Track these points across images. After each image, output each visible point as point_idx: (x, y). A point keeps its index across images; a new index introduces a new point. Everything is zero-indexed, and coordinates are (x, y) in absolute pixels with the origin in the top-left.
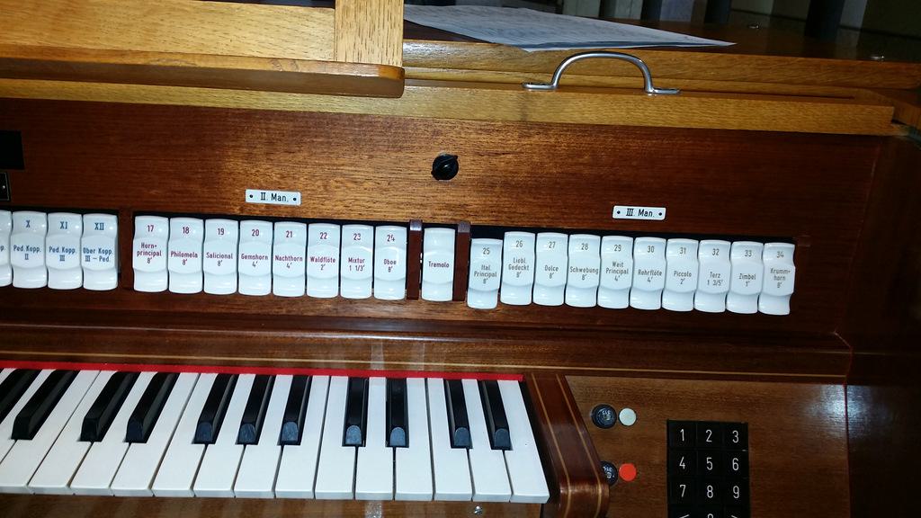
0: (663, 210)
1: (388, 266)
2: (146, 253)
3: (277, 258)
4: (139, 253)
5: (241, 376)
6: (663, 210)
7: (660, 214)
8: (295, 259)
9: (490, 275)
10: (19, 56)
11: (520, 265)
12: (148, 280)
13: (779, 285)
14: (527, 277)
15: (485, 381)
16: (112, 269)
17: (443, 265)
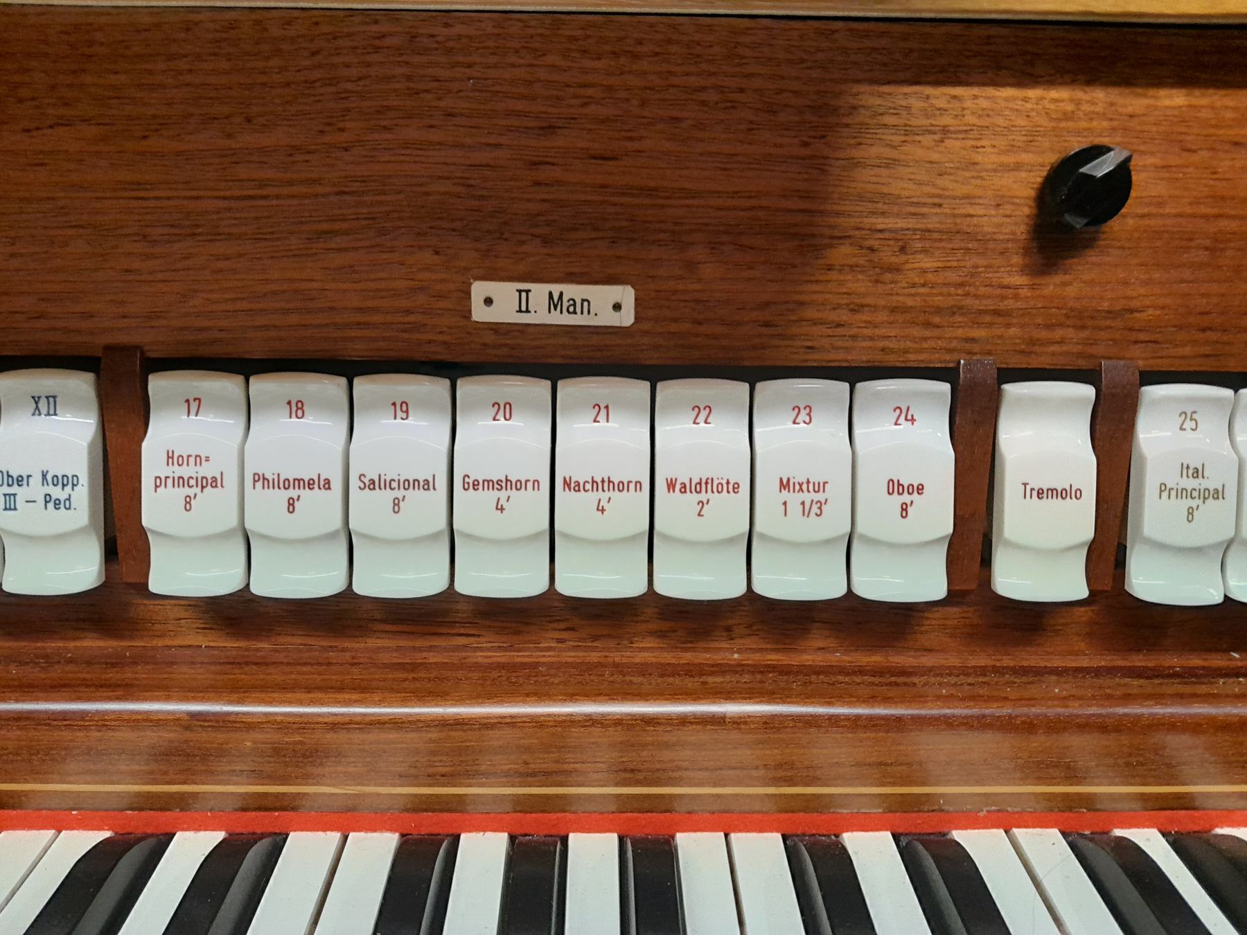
0: (626, 295)
1: (897, 500)
2: (181, 481)
3: (567, 484)
4: (159, 482)
6: (626, 295)
8: (622, 487)
14: (426, 511)
17: (1063, 494)
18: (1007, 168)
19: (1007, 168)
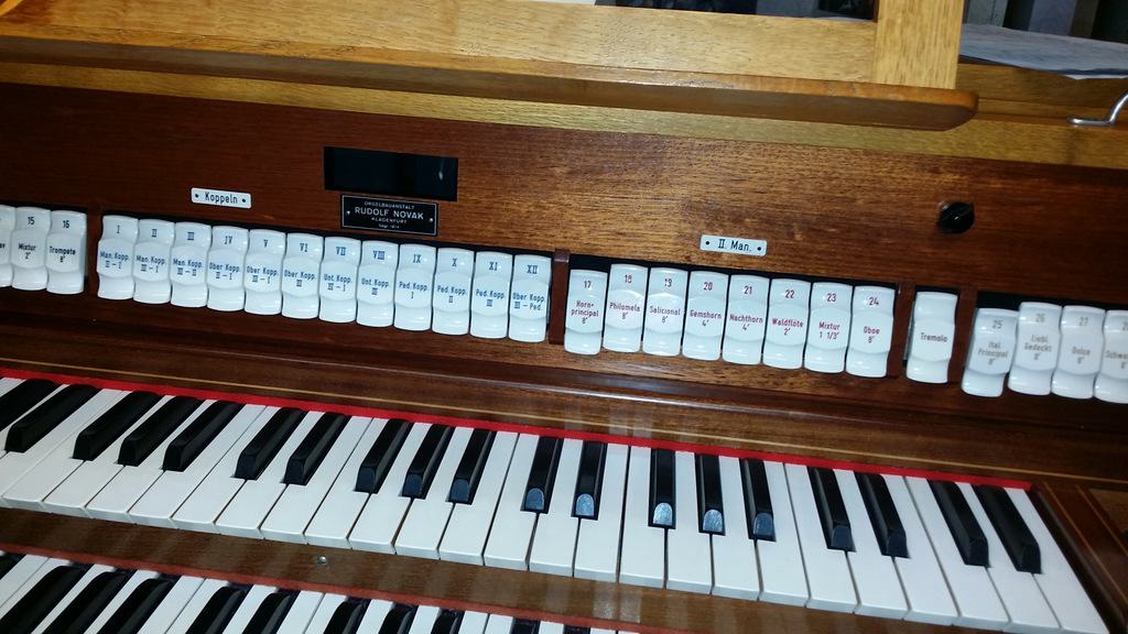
0: (763, 244)
1: (868, 335)
5: (416, 424)
6: (763, 244)
7: (759, 249)
9: (999, 355)
10: (538, 74)
11: (1040, 344)
12: (116, 286)
13: (1080, 360)
14: (797, 334)
15: (867, 474)
16: (542, 319)
17: (939, 339)
18: (924, 207)
19: (924, 207)
